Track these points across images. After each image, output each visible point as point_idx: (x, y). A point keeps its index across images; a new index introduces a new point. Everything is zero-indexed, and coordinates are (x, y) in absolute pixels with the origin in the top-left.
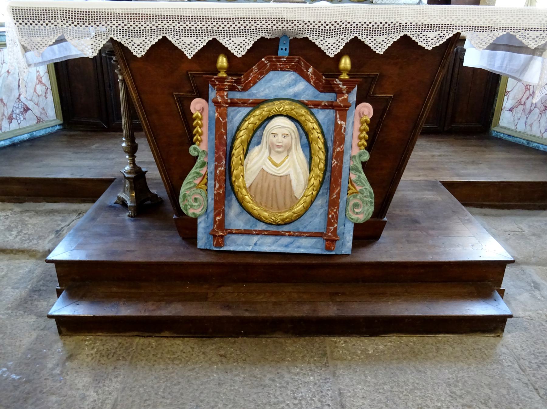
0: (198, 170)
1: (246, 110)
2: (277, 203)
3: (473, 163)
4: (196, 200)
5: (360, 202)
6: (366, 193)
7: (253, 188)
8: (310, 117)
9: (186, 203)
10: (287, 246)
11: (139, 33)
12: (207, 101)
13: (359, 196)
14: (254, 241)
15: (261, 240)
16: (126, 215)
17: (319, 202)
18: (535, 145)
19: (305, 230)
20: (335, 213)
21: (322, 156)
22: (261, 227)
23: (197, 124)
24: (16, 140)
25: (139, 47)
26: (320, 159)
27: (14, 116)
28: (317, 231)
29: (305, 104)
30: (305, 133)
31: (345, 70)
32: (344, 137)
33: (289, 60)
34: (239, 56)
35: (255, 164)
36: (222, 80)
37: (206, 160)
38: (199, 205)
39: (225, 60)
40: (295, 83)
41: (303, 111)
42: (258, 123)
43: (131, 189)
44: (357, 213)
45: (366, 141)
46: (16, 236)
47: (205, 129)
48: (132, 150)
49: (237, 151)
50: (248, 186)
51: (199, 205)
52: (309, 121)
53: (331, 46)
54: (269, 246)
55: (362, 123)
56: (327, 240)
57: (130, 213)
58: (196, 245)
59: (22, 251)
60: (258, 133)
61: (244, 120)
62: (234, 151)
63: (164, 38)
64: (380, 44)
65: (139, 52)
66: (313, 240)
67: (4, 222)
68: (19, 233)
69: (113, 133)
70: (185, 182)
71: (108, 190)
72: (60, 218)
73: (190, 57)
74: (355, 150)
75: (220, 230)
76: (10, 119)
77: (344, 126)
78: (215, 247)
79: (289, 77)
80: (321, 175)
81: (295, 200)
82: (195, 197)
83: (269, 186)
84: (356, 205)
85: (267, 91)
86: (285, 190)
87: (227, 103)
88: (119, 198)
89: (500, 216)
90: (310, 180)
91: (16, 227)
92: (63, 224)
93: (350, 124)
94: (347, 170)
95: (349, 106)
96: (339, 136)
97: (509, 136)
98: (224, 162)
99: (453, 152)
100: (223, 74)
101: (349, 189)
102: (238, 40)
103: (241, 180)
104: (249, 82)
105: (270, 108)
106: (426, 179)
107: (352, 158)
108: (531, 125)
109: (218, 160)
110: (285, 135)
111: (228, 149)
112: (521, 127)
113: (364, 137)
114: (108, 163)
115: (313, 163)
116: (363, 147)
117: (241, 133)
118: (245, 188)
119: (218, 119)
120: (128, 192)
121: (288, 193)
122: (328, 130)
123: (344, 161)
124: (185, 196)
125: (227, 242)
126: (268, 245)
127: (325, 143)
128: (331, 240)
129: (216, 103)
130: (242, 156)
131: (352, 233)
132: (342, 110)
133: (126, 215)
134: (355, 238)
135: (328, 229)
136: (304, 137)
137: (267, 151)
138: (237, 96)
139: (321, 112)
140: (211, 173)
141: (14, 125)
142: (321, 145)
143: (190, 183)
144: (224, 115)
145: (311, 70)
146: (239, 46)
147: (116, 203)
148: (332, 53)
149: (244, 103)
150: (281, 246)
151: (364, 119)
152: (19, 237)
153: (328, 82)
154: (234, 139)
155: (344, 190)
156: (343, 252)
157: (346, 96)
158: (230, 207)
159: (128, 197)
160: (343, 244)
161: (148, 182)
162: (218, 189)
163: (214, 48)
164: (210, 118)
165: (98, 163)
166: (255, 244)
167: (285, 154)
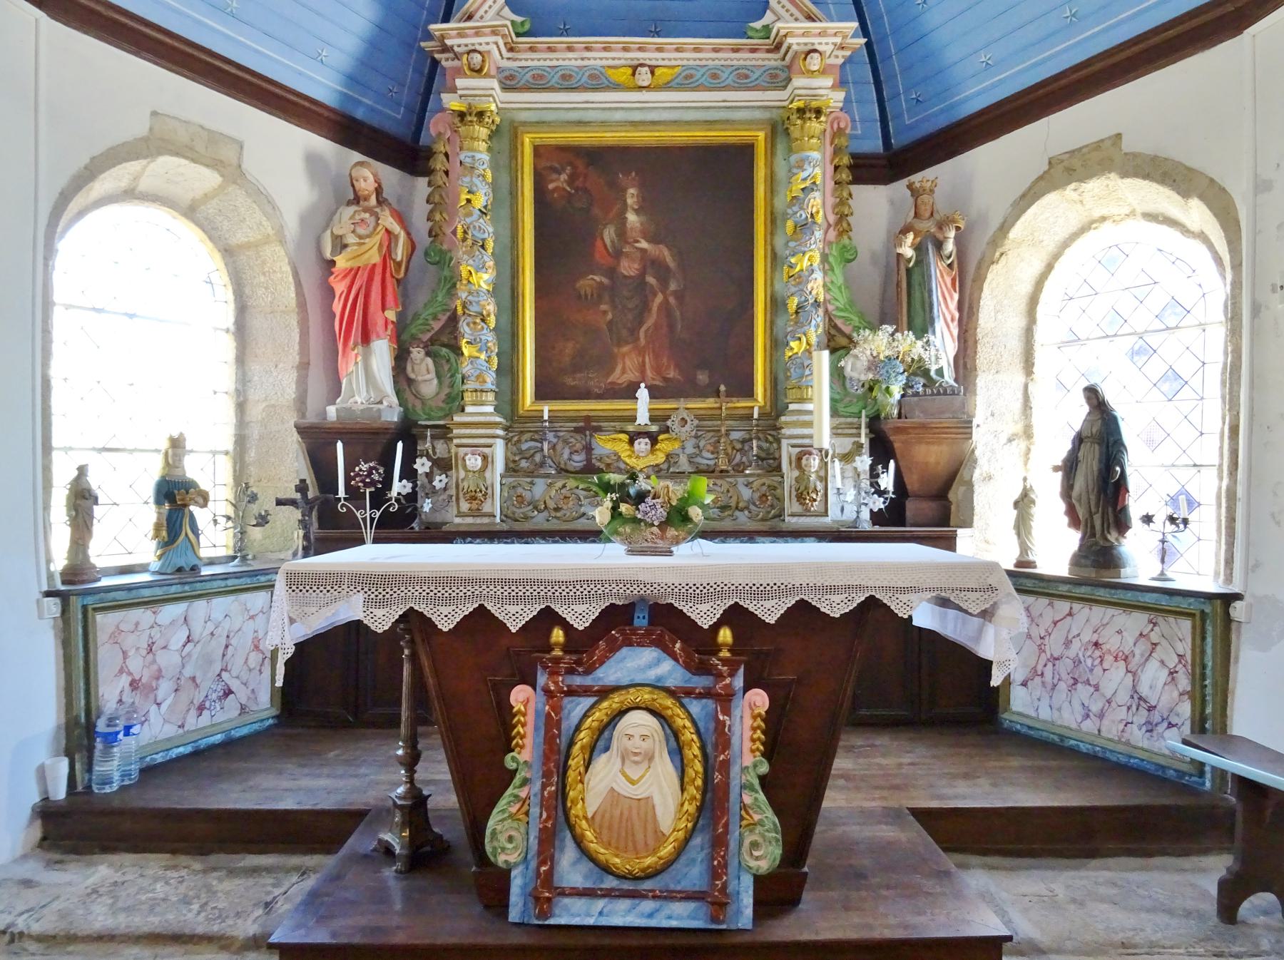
0: (516, 791)
1: (590, 701)
2: (634, 843)
3: (966, 776)
4: (510, 839)
5: (760, 840)
6: (769, 825)
7: (598, 819)
8: (678, 711)
9: (496, 844)
10: (650, 916)
11: (449, 600)
12: (535, 689)
13: (758, 829)
14: (599, 909)
15: (610, 907)
16: (389, 873)
17: (697, 841)
18: (1072, 742)
19: (679, 888)
20: (723, 857)
21: (699, 767)
22: (610, 883)
23: (519, 721)
24: (203, 743)
25: (446, 618)
26: (696, 773)
27: (207, 705)
28: (697, 889)
29: (671, 693)
30: (674, 734)
31: (725, 645)
32: (729, 739)
33: (648, 633)
34: (581, 628)
35: (601, 780)
36: (557, 660)
37: (528, 776)
38: (516, 848)
39: (561, 632)
40: (658, 662)
41: (669, 702)
42: (606, 719)
43: (403, 825)
44: (757, 858)
45: (763, 744)
46: (199, 913)
47: (529, 729)
48: (411, 761)
49: (576, 762)
50: (590, 815)
51: (516, 848)
52: (678, 716)
53: (704, 614)
54: (623, 916)
55: (754, 718)
56: (713, 904)
57: (399, 865)
58: (507, 918)
59: (208, 939)
60: (606, 734)
61: (586, 716)
62: (570, 762)
63: (481, 606)
64: (770, 611)
65: (445, 625)
66: (691, 906)
67: (176, 888)
68: (203, 906)
69: (363, 731)
70: (495, 811)
71: (361, 828)
72: (271, 881)
73: (514, 631)
74: (748, 758)
75: (547, 890)
76: (201, 708)
77: (728, 723)
78: (538, 918)
79: (649, 654)
80: (698, 797)
81: (661, 838)
82: (509, 835)
83: (622, 814)
84: (754, 845)
85: (619, 674)
86: (646, 821)
87: (563, 692)
88: (380, 841)
89: (1019, 868)
90: (682, 805)
91: (198, 897)
92: (277, 892)
93: (738, 719)
94: (737, 789)
95: (733, 695)
96: (722, 739)
97: (1029, 727)
98: (555, 779)
99: (934, 757)
100: (557, 652)
101: (742, 818)
102: (580, 608)
103: (579, 806)
104: (594, 663)
105: (622, 698)
106: (884, 804)
107: (744, 769)
108: (1059, 709)
109: (547, 775)
110: (644, 738)
111: (563, 759)
112: (1045, 714)
113: (759, 739)
114: (354, 782)
115: (686, 779)
116: (758, 754)
117: (582, 735)
118: (585, 818)
119: (549, 714)
120: (397, 830)
121: (650, 827)
122: (707, 729)
123: (732, 775)
124: (494, 833)
125: (557, 911)
126: (622, 914)
127: (703, 748)
128: (718, 902)
129: (547, 691)
130: (582, 769)
131: (751, 892)
132: (725, 700)
133: (389, 873)
134: (757, 903)
135: (713, 886)
136: (672, 739)
137: (619, 761)
138: (577, 681)
139: (695, 702)
140: (535, 795)
141: (205, 719)
142: (697, 752)
143: (503, 811)
144: (557, 709)
145: (678, 645)
146: (581, 616)
147: (375, 850)
148: (705, 623)
149: (585, 691)
150: (642, 915)
151: (756, 712)
152: (203, 914)
153: (701, 662)
154: (571, 744)
155: (734, 820)
156: (740, 926)
157: (728, 681)
158: (562, 850)
159: (395, 839)
160: (739, 912)
161: (430, 815)
162: (546, 821)
163: (548, 618)
164: (537, 712)
165: (340, 783)
166: (601, 913)
167: (645, 765)
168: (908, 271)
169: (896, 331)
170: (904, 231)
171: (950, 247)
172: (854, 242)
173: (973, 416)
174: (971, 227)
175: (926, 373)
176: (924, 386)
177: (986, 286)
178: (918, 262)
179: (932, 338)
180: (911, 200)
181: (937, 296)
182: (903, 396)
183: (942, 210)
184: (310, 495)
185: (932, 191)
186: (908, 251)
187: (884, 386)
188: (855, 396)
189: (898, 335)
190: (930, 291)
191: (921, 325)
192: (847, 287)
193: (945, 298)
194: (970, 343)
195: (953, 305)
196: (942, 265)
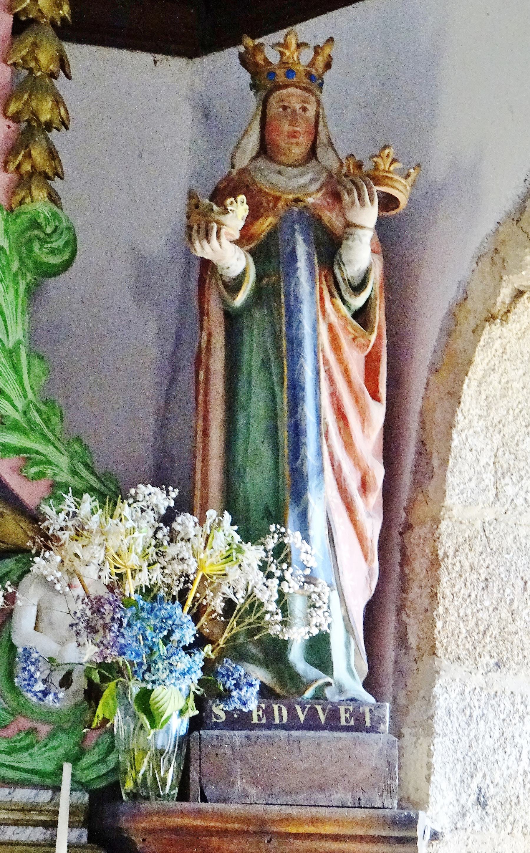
168: (232, 320)
169: (184, 505)
170: (220, 195)
171: (361, 255)
172: (71, 210)
173: (421, 804)
174: (430, 198)
175: (274, 653)
176: (265, 692)
177: (469, 390)
178: (259, 295)
179: (294, 538)
180: (252, 101)
181: (315, 407)
182: (196, 724)
183: (346, 138)
184: (130, 652)
185: (313, 81)
186: (233, 259)
187: (134, 688)
188: (47, 716)
189: (186, 522)
190: (295, 390)
191: (267, 510)
192: (36, 354)
193: (341, 415)
194: (419, 566)
195: (369, 440)
196: (338, 313)
